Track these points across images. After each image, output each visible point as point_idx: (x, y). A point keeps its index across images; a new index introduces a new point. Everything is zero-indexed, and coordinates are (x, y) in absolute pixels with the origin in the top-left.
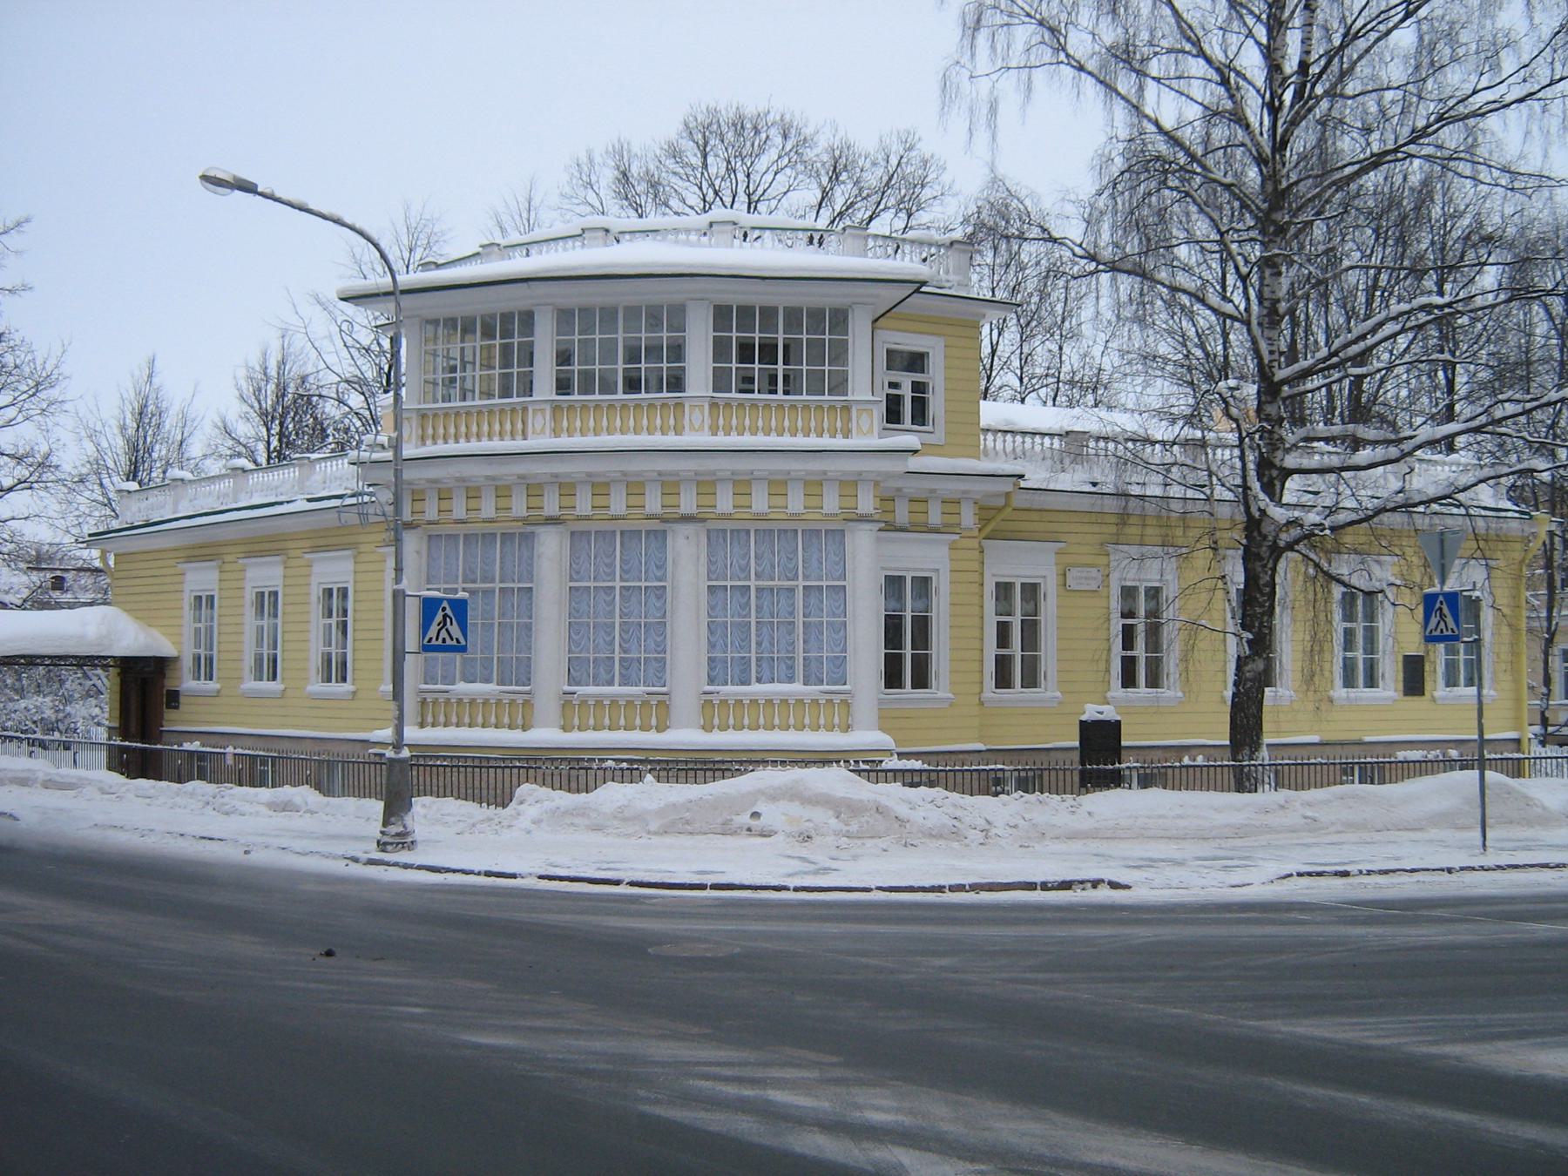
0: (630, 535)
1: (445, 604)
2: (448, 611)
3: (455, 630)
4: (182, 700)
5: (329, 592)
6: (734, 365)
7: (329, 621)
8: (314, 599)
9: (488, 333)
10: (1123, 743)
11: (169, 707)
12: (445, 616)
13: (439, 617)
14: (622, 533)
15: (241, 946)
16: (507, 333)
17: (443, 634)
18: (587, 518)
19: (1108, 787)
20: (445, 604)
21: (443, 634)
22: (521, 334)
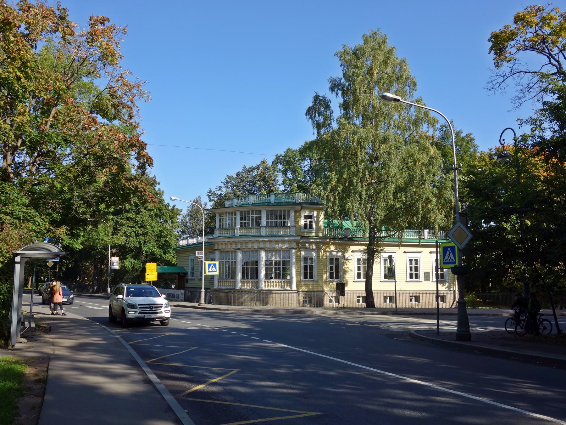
10: (373, 289)
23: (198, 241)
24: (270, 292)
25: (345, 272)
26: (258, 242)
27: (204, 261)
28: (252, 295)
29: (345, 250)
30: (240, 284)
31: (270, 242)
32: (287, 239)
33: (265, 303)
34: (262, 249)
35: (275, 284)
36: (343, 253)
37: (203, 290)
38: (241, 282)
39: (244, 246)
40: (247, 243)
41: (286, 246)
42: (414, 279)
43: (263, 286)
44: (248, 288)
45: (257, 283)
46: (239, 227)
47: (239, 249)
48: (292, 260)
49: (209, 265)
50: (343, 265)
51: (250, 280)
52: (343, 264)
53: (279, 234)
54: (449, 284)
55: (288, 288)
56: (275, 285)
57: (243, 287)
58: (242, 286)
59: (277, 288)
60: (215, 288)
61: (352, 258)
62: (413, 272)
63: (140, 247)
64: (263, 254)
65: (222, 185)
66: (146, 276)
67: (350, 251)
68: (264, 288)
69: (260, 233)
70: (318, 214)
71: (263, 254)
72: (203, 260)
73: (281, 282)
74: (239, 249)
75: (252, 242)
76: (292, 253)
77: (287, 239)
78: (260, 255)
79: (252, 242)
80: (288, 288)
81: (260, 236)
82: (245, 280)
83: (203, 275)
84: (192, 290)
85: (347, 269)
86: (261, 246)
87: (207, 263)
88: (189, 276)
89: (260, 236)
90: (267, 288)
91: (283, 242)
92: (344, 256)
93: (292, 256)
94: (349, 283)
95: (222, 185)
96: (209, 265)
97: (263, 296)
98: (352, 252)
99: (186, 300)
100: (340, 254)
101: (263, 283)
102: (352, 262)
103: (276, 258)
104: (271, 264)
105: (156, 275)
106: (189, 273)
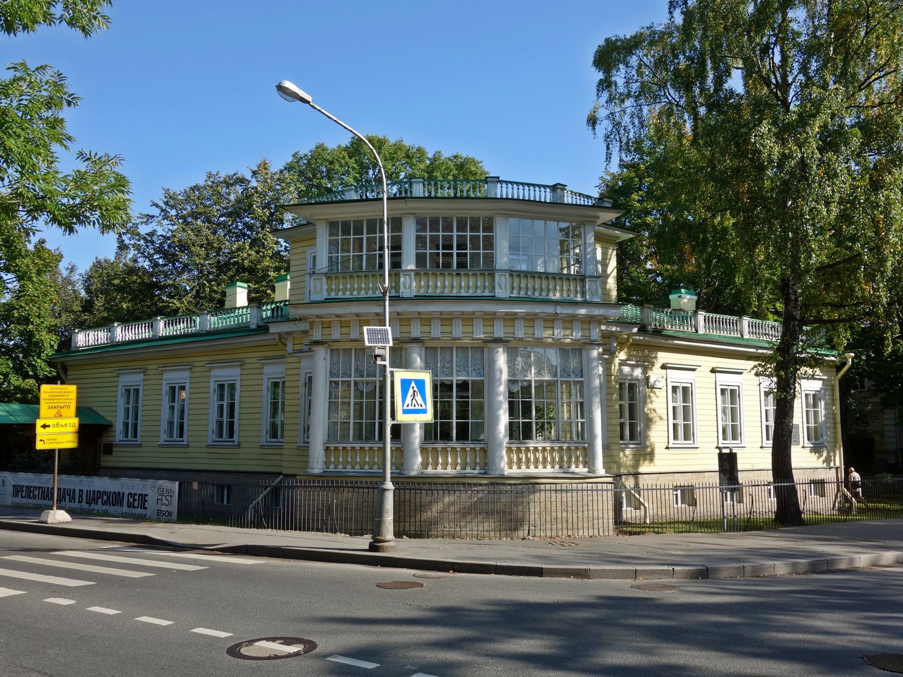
0: (463, 349)
1: (413, 384)
2: (416, 389)
3: (419, 398)
4: (114, 449)
5: (221, 387)
6: (481, 251)
7: (221, 403)
8: (265, 388)
9: (346, 232)
10: (793, 466)
11: (104, 453)
12: (414, 391)
13: (411, 392)
14: (457, 348)
15: (694, 589)
16: (358, 231)
17: (414, 402)
18: (438, 339)
19: (139, 522)
20: (413, 384)
21: (414, 402)
22: (343, 234)
23: (113, 337)
24: (530, 484)
25: (649, 421)
26: (490, 318)
27: (388, 369)
28: (464, 498)
29: (646, 364)
30: (419, 459)
31: (531, 319)
32: (583, 311)
33: (511, 522)
34: (498, 341)
35: (540, 456)
36: (645, 370)
37: (389, 485)
38: (423, 450)
39: (436, 330)
40: (447, 319)
41: (577, 335)
42: (681, 441)
43: (506, 465)
44: (449, 471)
45: (486, 455)
46: (412, 267)
47: (416, 340)
48: (590, 381)
49: (406, 383)
50: (645, 403)
51: (459, 446)
52: (645, 399)
53: (551, 296)
54: (828, 453)
55: (582, 470)
56: (532, 462)
57: (430, 470)
58: (425, 465)
59: (549, 470)
60: (413, 473)
61: (661, 384)
62: (680, 421)
63: (791, 84)
64: (501, 359)
65: (156, 212)
66: (39, 430)
67: (658, 365)
68: (507, 472)
69: (493, 288)
70: (604, 254)
71: (501, 359)
72: (387, 363)
73: (561, 448)
74: (416, 340)
75: (468, 319)
76: (590, 360)
77: (583, 311)
78: (492, 362)
79: (468, 319)
80: (582, 470)
81: (493, 299)
82: (439, 446)
83: (389, 423)
84: (228, 480)
85: (652, 415)
86: (499, 331)
87: (400, 375)
88: (118, 434)
89: (493, 299)
90: (515, 471)
91: (570, 321)
92: (647, 379)
93: (590, 370)
94: (656, 451)
95: (156, 212)
96: (406, 383)
97: (505, 504)
98: (664, 367)
99: (186, 515)
100: (638, 372)
101: (504, 453)
102: (661, 394)
103: (539, 373)
104: (526, 390)
105: (76, 428)
106: (119, 427)
